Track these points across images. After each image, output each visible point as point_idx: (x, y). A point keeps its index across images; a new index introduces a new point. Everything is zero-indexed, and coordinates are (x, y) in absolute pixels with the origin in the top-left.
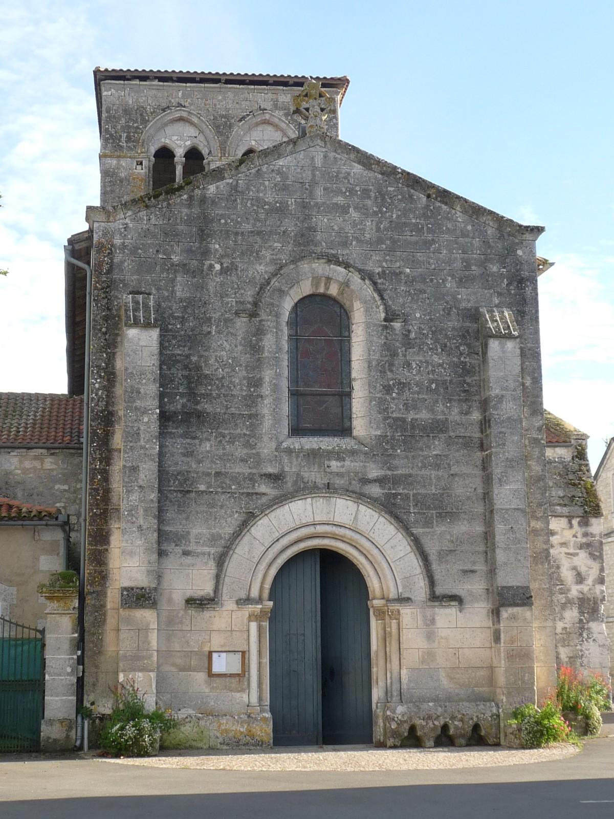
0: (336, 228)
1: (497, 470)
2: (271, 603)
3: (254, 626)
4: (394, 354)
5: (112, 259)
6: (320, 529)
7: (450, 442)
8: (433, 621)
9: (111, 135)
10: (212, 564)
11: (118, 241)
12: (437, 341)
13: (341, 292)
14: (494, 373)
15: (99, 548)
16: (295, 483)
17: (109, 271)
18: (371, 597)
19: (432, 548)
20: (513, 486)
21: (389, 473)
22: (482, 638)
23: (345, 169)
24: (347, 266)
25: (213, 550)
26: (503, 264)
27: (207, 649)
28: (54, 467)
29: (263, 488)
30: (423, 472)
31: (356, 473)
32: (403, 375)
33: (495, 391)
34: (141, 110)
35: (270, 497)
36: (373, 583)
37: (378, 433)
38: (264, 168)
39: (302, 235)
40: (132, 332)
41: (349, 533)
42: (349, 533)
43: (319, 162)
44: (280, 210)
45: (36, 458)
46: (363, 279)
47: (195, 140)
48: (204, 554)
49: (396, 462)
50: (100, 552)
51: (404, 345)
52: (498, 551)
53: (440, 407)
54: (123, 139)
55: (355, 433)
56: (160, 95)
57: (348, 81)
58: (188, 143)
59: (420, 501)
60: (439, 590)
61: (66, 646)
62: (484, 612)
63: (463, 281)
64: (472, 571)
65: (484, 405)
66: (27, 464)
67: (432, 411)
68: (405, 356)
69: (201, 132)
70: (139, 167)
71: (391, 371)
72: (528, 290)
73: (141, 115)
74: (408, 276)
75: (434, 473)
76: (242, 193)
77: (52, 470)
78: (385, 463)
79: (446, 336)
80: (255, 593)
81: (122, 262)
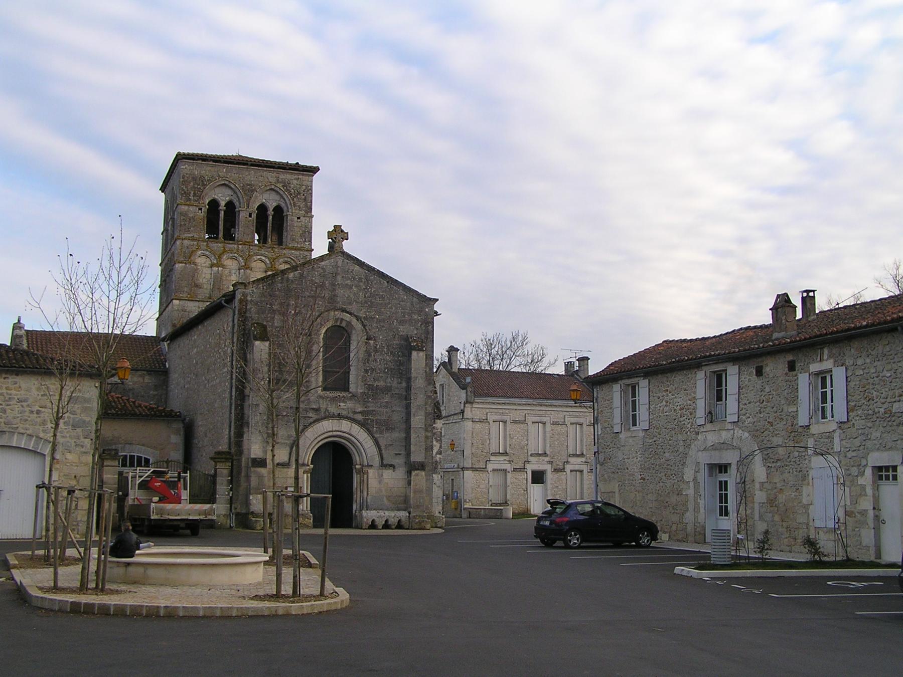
0: (347, 296)
1: (413, 410)
2: (312, 466)
3: (305, 475)
4: (370, 355)
5: (246, 307)
6: (335, 433)
7: (392, 396)
8: (382, 475)
9: (185, 192)
10: (288, 448)
11: (249, 298)
12: (388, 350)
13: (347, 325)
14: (414, 365)
15: (239, 439)
16: (325, 413)
17: (245, 313)
18: (354, 464)
19: (382, 443)
20: (420, 417)
21: (365, 409)
22: (402, 484)
23: (351, 268)
24: (350, 314)
25: (288, 442)
26: (419, 315)
27: (285, 486)
28: (150, 381)
29: (311, 415)
30: (380, 409)
31: (351, 409)
32: (373, 365)
33: (413, 375)
34: (202, 178)
35: (314, 419)
36: (356, 458)
37: (362, 391)
38: (315, 266)
39: (331, 299)
40: (257, 343)
41: (347, 435)
42: (347, 435)
43: (340, 264)
44: (322, 286)
45: (140, 376)
46: (358, 320)
47: (232, 198)
48: (284, 443)
49: (369, 404)
50: (240, 441)
51: (374, 351)
52: (411, 446)
53: (389, 380)
54: (192, 195)
55: (350, 390)
56: (213, 169)
57: (319, 169)
58: (228, 198)
59: (378, 422)
60: (385, 462)
61: (225, 483)
62: (404, 472)
63: (402, 322)
64: (400, 454)
65: (409, 380)
66: (135, 379)
67: (386, 382)
68: (374, 356)
69: (235, 193)
70: (200, 211)
71: (368, 363)
72: (430, 328)
73: (202, 181)
74: (377, 319)
75: (385, 410)
76: (305, 277)
77: (149, 383)
78: (364, 404)
79: (393, 347)
80: (306, 462)
81: (251, 308)
